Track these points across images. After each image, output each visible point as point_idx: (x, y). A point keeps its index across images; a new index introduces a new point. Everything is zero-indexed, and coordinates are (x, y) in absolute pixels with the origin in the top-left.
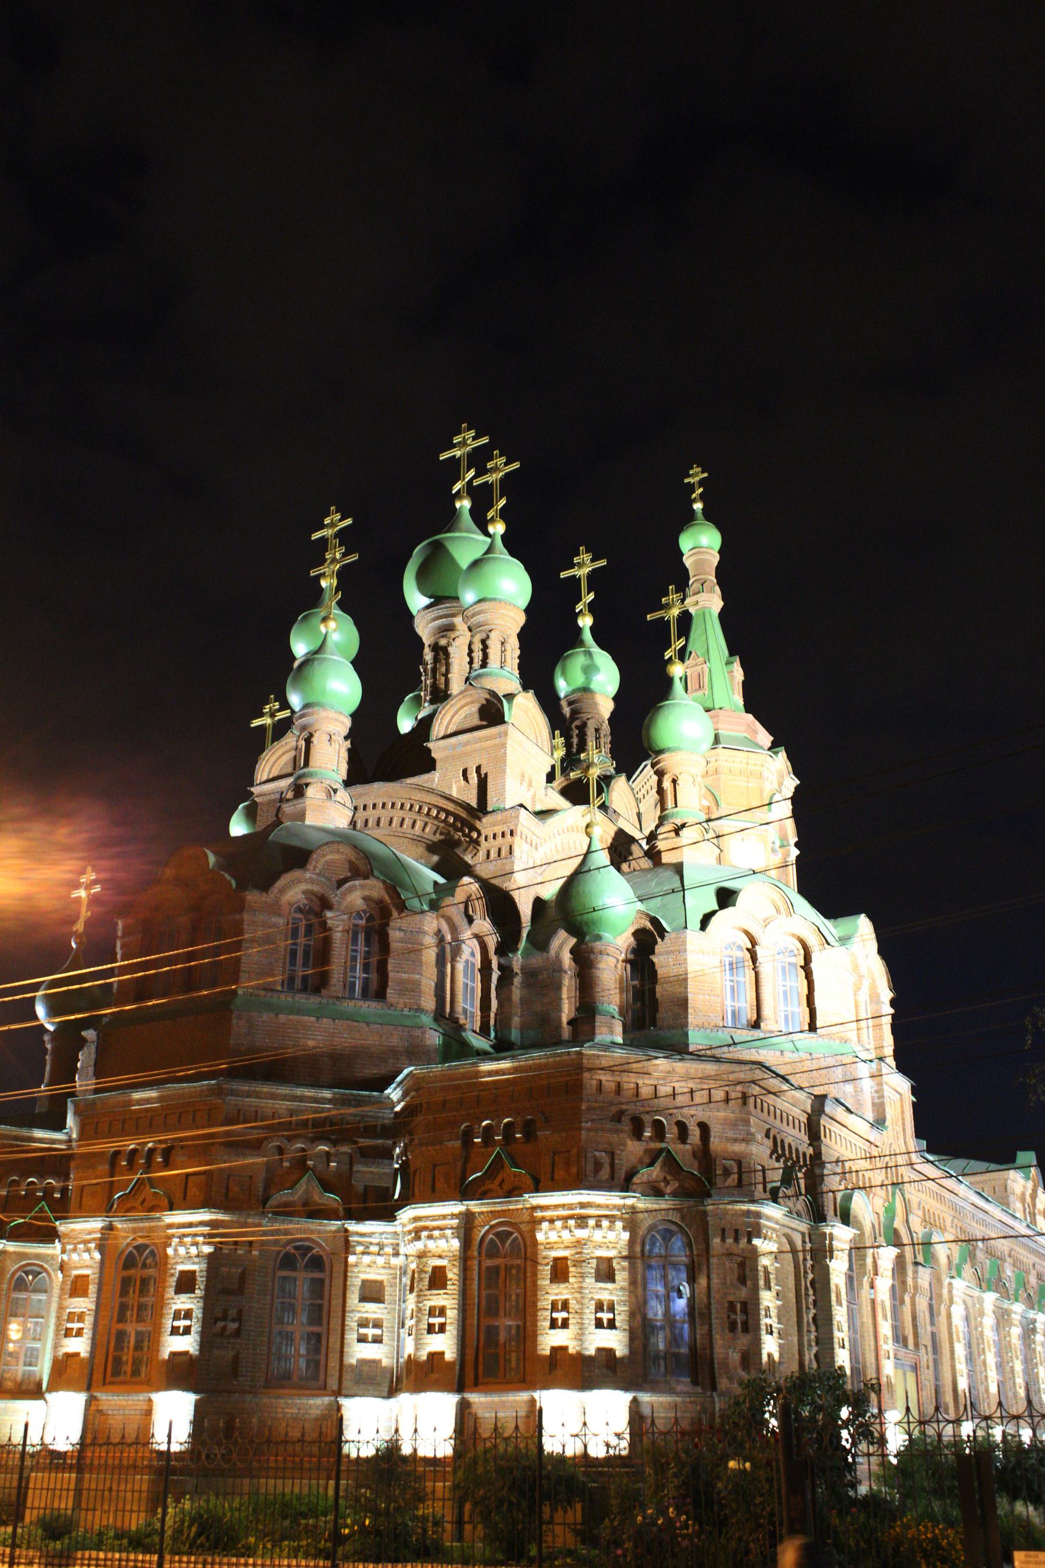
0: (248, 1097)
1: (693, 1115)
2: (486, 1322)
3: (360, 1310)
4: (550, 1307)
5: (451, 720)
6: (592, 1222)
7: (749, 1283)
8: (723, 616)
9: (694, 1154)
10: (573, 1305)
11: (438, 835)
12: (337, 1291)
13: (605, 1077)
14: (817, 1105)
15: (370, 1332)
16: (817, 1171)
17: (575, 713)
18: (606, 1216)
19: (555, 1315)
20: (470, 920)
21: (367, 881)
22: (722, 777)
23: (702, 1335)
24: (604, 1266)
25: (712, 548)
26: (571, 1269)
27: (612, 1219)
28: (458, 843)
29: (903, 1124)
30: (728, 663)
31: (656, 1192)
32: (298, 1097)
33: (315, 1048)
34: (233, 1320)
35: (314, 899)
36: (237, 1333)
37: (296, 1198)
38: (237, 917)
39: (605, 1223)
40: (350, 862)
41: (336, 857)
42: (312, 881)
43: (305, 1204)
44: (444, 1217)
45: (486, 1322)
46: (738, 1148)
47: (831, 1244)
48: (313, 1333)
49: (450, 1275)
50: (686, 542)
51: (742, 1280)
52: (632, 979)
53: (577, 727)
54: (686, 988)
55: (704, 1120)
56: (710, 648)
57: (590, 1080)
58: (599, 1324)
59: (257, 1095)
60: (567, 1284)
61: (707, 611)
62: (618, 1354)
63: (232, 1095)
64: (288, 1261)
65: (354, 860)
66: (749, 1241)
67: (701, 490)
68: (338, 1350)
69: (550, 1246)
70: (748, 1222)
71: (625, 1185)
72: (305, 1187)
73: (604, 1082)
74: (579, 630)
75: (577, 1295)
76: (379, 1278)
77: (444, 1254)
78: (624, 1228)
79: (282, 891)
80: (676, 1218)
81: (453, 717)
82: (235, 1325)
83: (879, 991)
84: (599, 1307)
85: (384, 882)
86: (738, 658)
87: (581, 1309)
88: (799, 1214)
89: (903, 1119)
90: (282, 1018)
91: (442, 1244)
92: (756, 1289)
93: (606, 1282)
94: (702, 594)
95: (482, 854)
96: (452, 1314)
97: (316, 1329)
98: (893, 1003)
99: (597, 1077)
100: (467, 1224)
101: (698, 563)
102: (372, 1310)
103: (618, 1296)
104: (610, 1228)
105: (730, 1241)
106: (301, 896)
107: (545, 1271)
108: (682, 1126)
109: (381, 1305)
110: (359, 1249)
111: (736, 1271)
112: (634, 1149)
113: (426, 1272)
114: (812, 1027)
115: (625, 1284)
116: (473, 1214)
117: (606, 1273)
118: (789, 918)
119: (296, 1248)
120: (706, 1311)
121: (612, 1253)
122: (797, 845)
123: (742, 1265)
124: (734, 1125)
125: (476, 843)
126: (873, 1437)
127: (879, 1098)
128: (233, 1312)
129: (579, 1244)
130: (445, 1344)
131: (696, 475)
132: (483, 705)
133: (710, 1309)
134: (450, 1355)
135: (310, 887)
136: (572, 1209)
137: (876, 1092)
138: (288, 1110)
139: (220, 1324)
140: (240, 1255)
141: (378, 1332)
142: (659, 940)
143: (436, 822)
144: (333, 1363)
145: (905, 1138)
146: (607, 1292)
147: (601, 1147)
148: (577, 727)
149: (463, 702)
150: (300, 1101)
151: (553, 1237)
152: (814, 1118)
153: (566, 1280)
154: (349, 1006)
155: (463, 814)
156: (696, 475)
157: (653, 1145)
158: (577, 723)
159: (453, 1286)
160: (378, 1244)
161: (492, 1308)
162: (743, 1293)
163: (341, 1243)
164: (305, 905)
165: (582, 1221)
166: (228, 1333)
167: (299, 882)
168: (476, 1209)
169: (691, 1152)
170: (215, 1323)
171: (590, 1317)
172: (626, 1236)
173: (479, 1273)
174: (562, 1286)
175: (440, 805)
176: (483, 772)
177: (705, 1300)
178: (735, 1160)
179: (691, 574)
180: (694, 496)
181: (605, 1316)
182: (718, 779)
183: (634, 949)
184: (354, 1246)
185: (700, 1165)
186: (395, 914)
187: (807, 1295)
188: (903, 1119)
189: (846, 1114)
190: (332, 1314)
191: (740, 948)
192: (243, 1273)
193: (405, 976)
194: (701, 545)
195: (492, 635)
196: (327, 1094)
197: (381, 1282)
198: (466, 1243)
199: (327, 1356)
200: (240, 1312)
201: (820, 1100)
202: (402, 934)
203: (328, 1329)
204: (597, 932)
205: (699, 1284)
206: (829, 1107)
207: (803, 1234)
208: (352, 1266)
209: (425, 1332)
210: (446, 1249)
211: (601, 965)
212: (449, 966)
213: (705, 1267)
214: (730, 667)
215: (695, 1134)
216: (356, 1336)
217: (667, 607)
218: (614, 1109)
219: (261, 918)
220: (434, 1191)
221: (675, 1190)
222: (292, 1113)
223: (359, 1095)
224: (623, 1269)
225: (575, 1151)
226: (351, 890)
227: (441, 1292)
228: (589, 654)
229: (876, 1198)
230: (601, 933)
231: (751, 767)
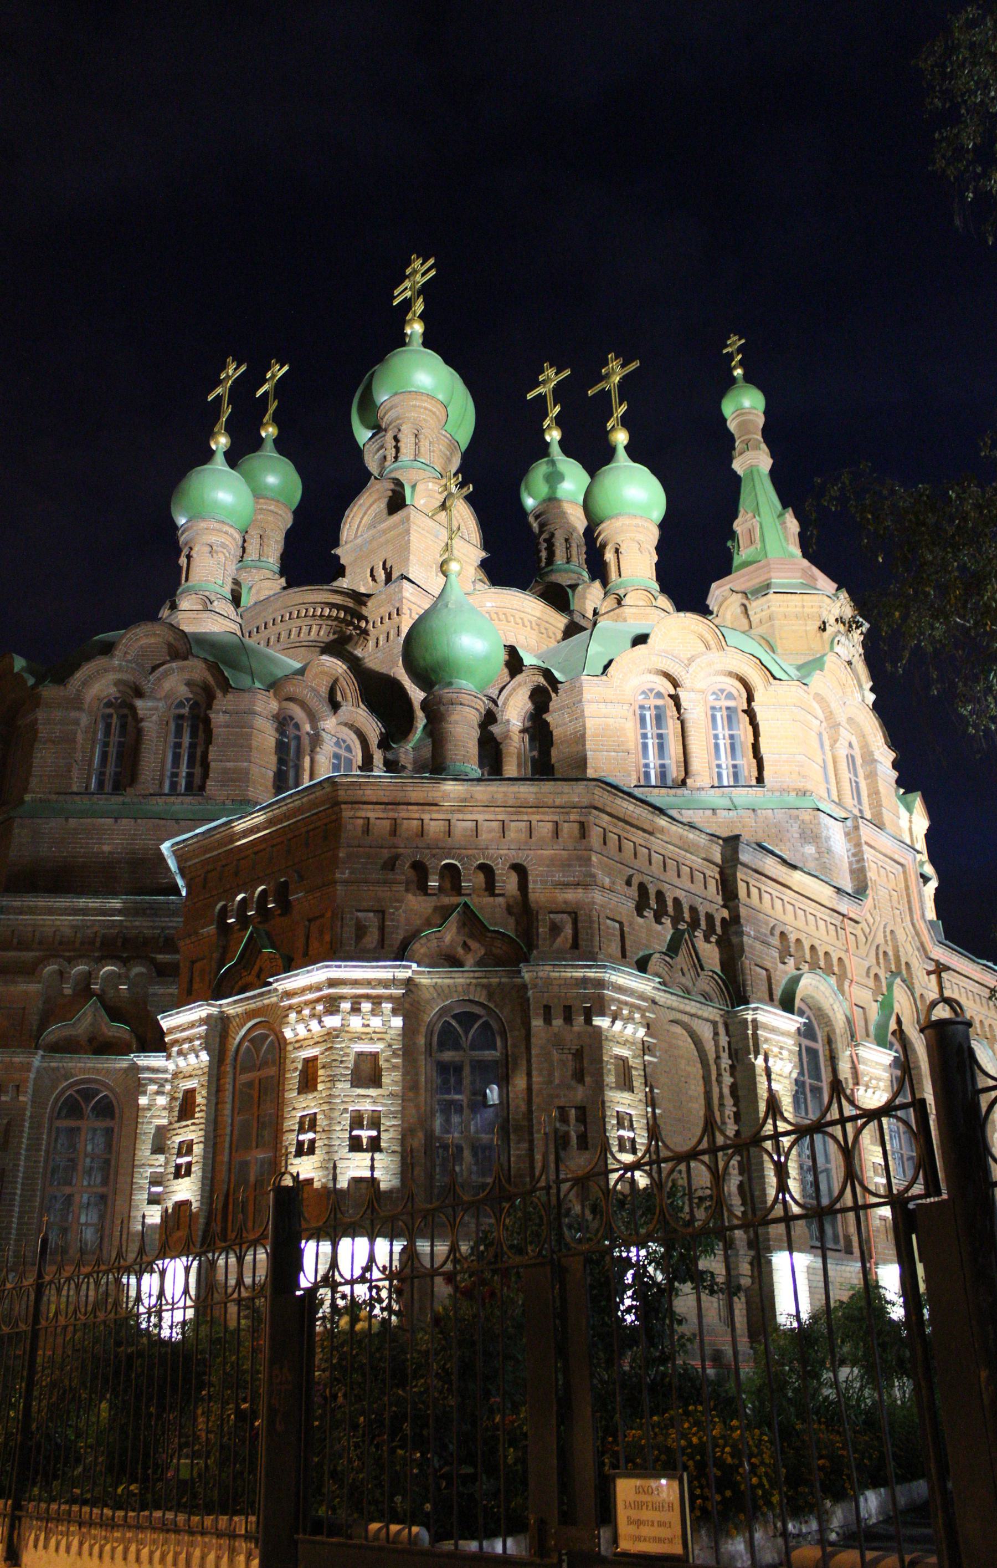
0: (21, 914)
1: (501, 856)
4: (296, 1127)
5: (360, 522)
6: (346, 1006)
7: (588, 1079)
8: (774, 473)
9: (509, 910)
10: (321, 1121)
11: (331, 635)
13: (372, 813)
14: (729, 853)
16: (735, 940)
17: (542, 526)
18: (367, 997)
19: (301, 1137)
20: (335, 706)
21: (186, 662)
22: (777, 623)
23: (519, 1156)
24: (366, 1067)
25: (755, 408)
26: (321, 1072)
27: (377, 1001)
28: (350, 637)
29: (909, 902)
30: (780, 515)
31: (452, 961)
32: (82, 910)
33: (110, 853)
35: (129, 691)
39: (366, 1006)
40: (170, 645)
41: (152, 640)
42: (120, 669)
43: (91, 1040)
44: (192, 1025)
46: (571, 896)
47: (755, 1035)
50: (728, 408)
51: (579, 1076)
52: (531, 750)
53: (545, 540)
54: (584, 745)
55: (519, 861)
56: (760, 504)
57: (352, 818)
58: (356, 1145)
59: (32, 911)
60: (315, 1094)
61: (754, 469)
62: (383, 1186)
64: (72, 1108)
65: (173, 642)
66: (588, 1021)
67: (740, 357)
69: (300, 1044)
70: (585, 995)
71: (401, 954)
73: (372, 821)
74: (547, 445)
75: (325, 1107)
77: (194, 1073)
78: (395, 1012)
79: (85, 684)
80: (481, 997)
81: (362, 519)
83: (873, 748)
84: (357, 1121)
85: (205, 660)
86: (790, 510)
87: (329, 1125)
88: (706, 996)
89: (908, 896)
90: (73, 822)
92: (599, 1087)
93: (369, 1088)
94: (747, 453)
95: (371, 644)
98: (895, 765)
99: (362, 814)
101: (743, 425)
103: (384, 1105)
104: (373, 1013)
105: (558, 1022)
106: (113, 690)
107: (293, 1078)
108: (487, 870)
111: (570, 1065)
112: (416, 906)
114: (760, 780)
115: (397, 1089)
116: (228, 1017)
117: (367, 1073)
118: (721, 652)
120: (526, 1123)
121: (377, 1047)
122: (872, 690)
123: (578, 1055)
124: (566, 865)
125: (365, 632)
126: (714, 1283)
127: (858, 861)
129: (331, 1036)
131: (734, 343)
133: (530, 1120)
136: (320, 990)
137: (854, 855)
138: (73, 927)
142: (553, 695)
143: (330, 623)
145: (912, 920)
146: (367, 1101)
147: (365, 905)
148: (545, 540)
149: (371, 501)
150: (84, 915)
151: (302, 1031)
152: (728, 871)
153: (315, 1089)
154: (159, 804)
155: (350, 603)
156: (734, 343)
157: (447, 900)
158: (545, 536)
161: (243, 1141)
162: (580, 1094)
164: (116, 699)
165: (332, 1005)
167: (106, 671)
168: (231, 1011)
169: (504, 906)
171: (341, 1136)
172: (398, 1022)
173: (234, 1093)
174: (310, 1096)
175: (330, 601)
176: (388, 566)
177: (523, 1108)
178: (569, 913)
179: (736, 436)
180: (733, 363)
181: (365, 1134)
182: (772, 625)
183: (531, 715)
184: (146, 1085)
185: (518, 923)
186: (219, 694)
187: (722, 1105)
188: (908, 896)
189: (789, 871)
191: (659, 695)
192: (9, 1124)
193: (230, 765)
194: (745, 407)
195: (403, 428)
196: (116, 903)
201: (732, 843)
202: (227, 717)
204: (448, 680)
205: (514, 1086)
206: (745, 856)
207: (715, 1024)
208: (144, 1109)
209: (171, 1176)
210: (197, 1066)
211: (454, 717)
212: (307, 760)
213: (524, 1062)
214: (781, 518)
215: (509, 883)
216: (146, 1196)
217: (608, 376)
218: (386, 853)
219: (58, 714)
221: (482, 958)
222: (76, 928)
223: (156, 902)
224: (395, 1067)
225: (329, 914)
226: (166, 674)
227: (189, 1122)
228: (553, 463)
229: (854, 986)
230: (453, 680)
231: (807, 610)
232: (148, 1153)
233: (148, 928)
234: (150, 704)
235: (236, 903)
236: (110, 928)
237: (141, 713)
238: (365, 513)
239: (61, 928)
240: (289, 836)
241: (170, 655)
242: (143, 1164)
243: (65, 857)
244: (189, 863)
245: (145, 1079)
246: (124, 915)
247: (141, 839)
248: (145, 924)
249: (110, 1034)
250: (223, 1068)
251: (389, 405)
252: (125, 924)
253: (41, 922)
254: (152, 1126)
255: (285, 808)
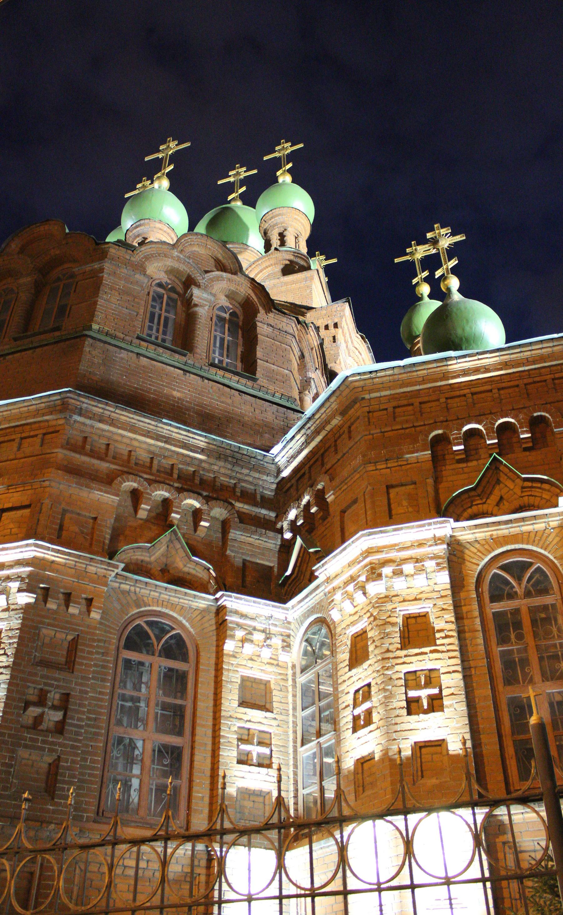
0: (100, 421)
2: (506, 693)
3: (237, 718)
12: (206, 690)
15: (255, 750)
32: (165, 437)
33: (179, 399)
34: (54, 708)
36: (60, 728)
37: (153, 558)
38: (96, 266)
42: (179, 259)
45: (506, 693)
48: (165, 746)
49: (438, 624)
63: (80, 415)
64: (137, 639)
65: (221, 258)
68: (208, 773)
72: (163, 548)
76: (264, 677)
77: (423, 596)
82: (57, 716)
91: (420, 583)
96: (452, 682)
97: (173, 740)
100: (455, 556)
102: (255, 719)
109: (268, 714)
110: (240, 634)
113: (393, 624)
119: (150, 624)
128: (54, 696)
130: (448, 727)
132: (286, 265)
134: (455, 747)
135: (176, 265)
139: (34, 711)
140: (73, 615)
141: (265, 751)
144: (201, 793)
149: (267, 263)
150: (165, 442)
159: (448, 642)
160: (263, 631)
163: (210, 623)
166: (44, 726)
167: (166, 256)
170: (25, 709)
184: (233, 629)
190: (198, 721)
192: (74, 643)
197: (267, 683)
198: (457, 584)
199: (191, 781)
200: (66, 697)
202: (270, 329)
203: (193, 742)
216: (235, 754)
219: (124, 271)
220: (391, 516)
227: (427, 650)
232: (236, 704)
233: (225, 475)
234: (205, 295)
235: (462, 432)
236: (188, 464)
237: (195, 300)
238: (261, 271)
239: (138, 449)
240: (526, 381)
241: (216, 267)
242: (231, 717)
243: (137, 388)
244: (373, 395)
245: (232, 622)
246: (208, 456)
247: (207, 397)
248: (223, 471)
249: (186, 569)
250: (463, 595)
251: (277, 213)
252: (203, 465)
253: (119, 439)
254: (238, 676)
255: (529, 353)
